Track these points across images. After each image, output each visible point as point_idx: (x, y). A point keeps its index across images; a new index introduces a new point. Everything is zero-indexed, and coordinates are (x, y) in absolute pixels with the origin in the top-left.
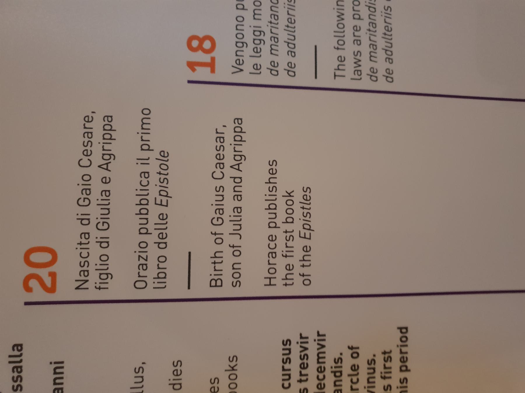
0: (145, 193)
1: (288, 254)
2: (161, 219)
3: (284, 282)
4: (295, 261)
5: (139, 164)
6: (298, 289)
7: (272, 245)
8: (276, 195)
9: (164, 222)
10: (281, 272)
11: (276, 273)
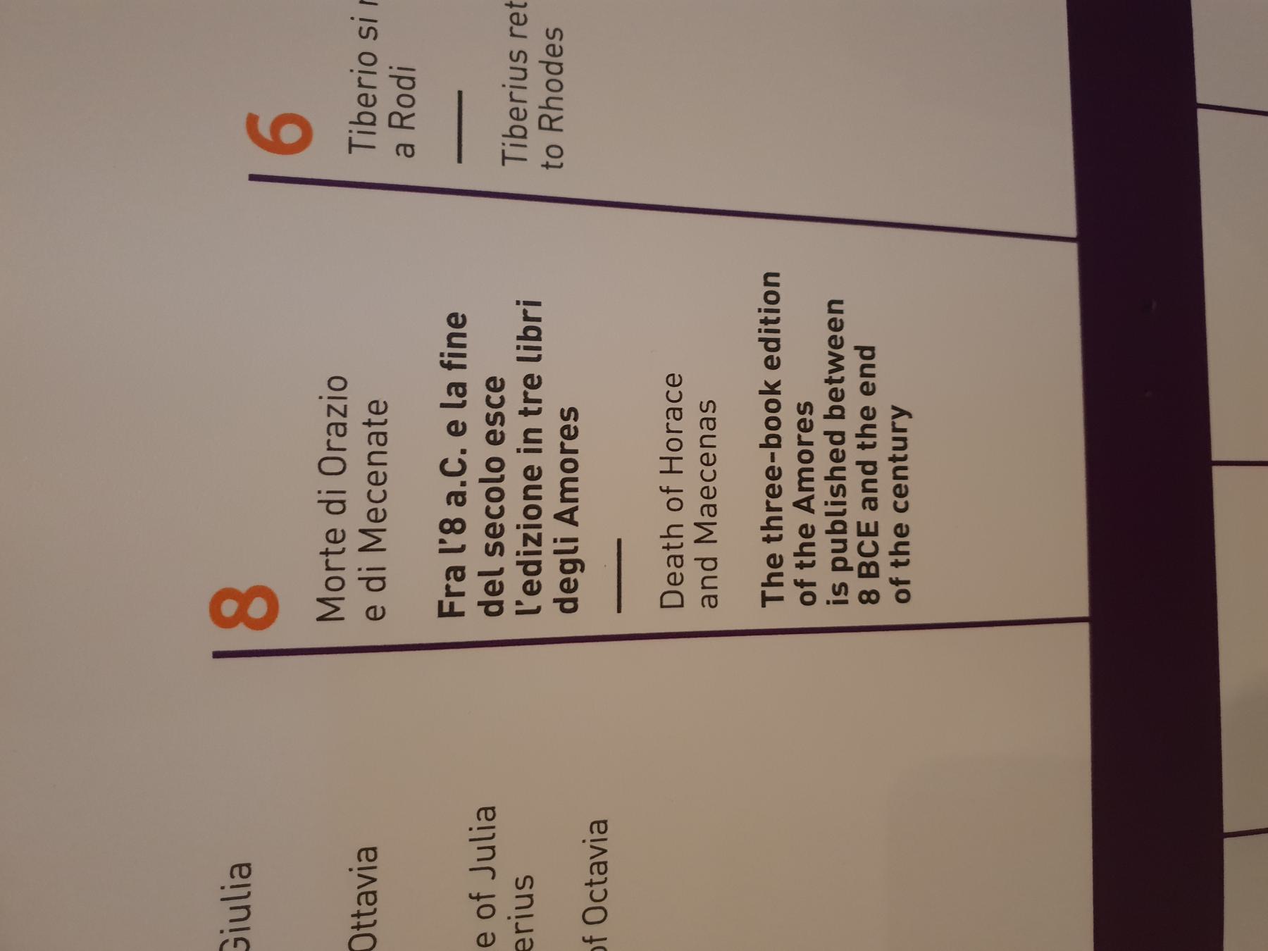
2: (372, 521)
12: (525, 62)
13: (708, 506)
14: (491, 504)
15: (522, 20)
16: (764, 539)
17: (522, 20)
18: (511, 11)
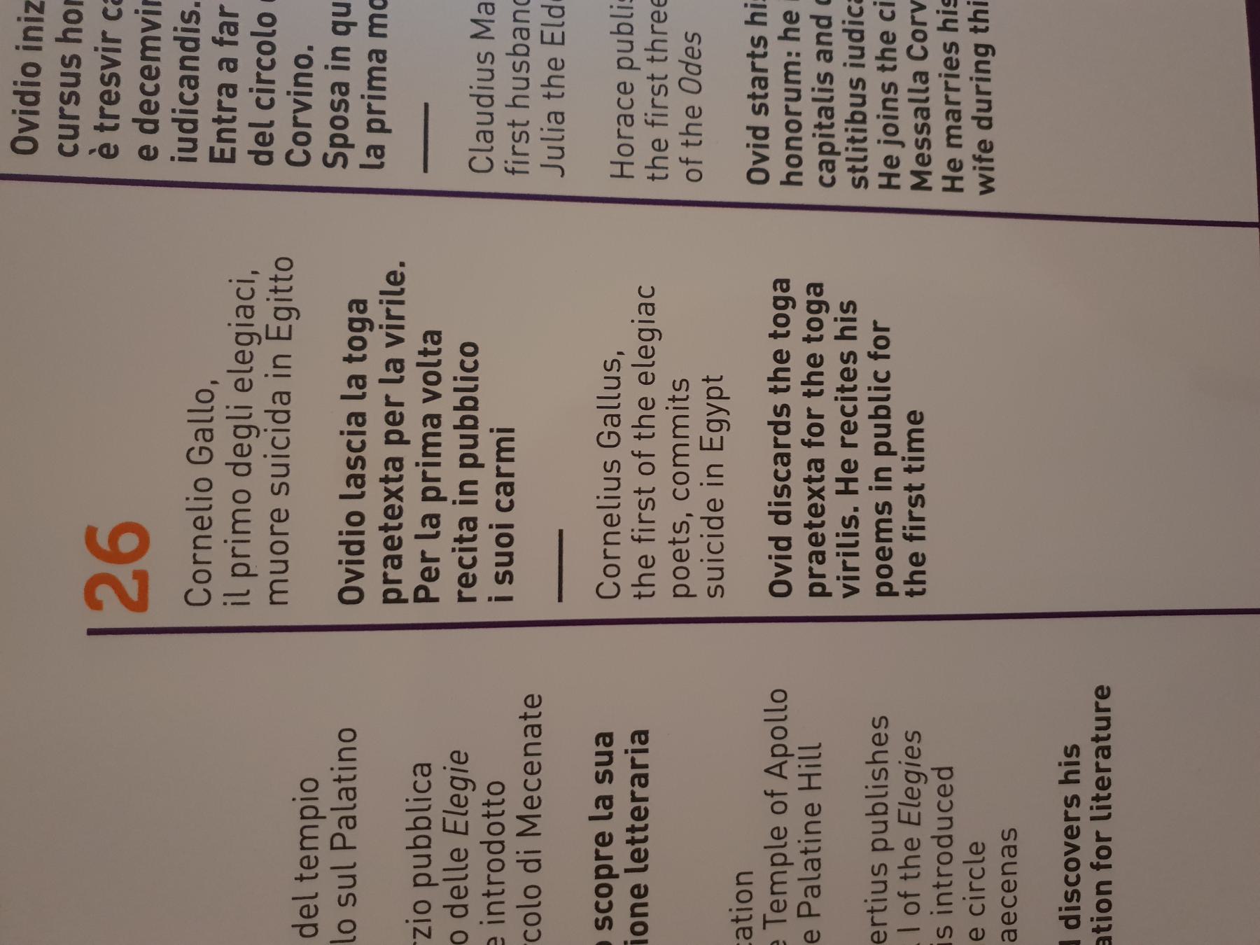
0: (424, 805)
1: (657, 119)
3: (650, 172)
4: (671, 133)
5: (229, 604)
6: (676, 187)
7: (625, 101)
8: (632, 8)
9: (462, 865)
10: (644, 154)
11: (1002, 864)
12: (492, 62)
13: (1009, 931)
14: (600, 900)
15: (662, 17)
16: (805, 394)
17: (662, 17)
18: (384, 535)
